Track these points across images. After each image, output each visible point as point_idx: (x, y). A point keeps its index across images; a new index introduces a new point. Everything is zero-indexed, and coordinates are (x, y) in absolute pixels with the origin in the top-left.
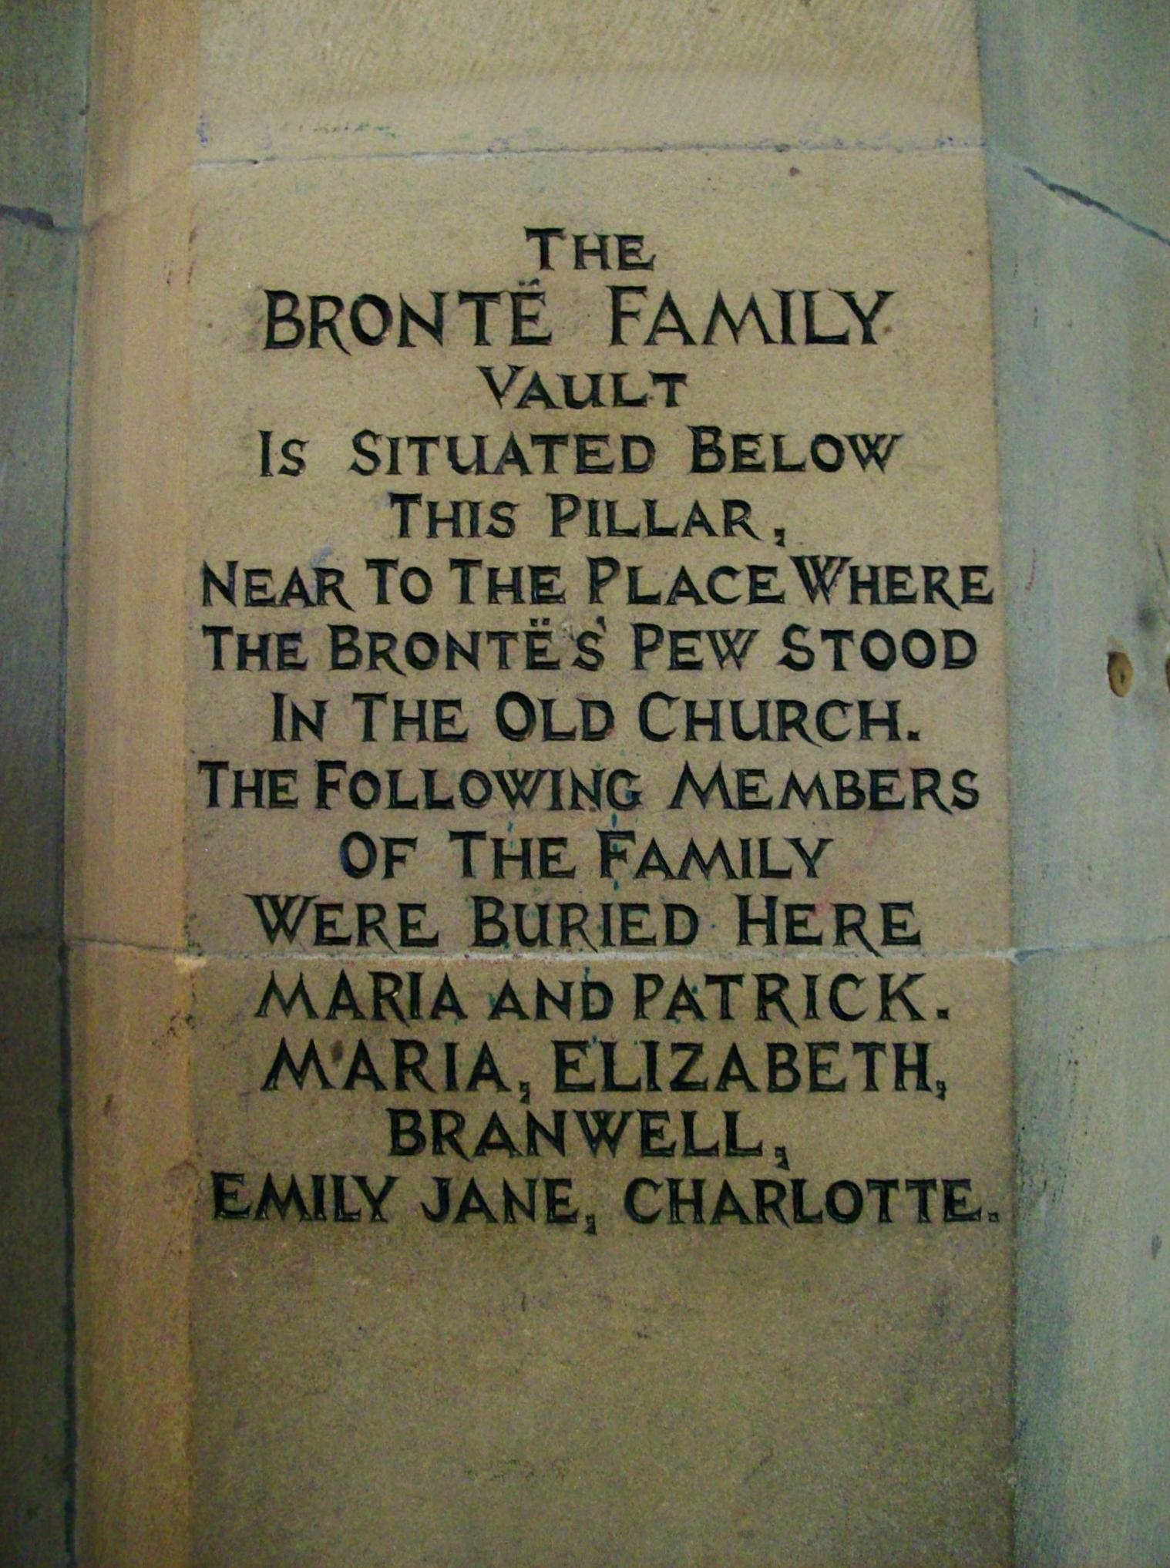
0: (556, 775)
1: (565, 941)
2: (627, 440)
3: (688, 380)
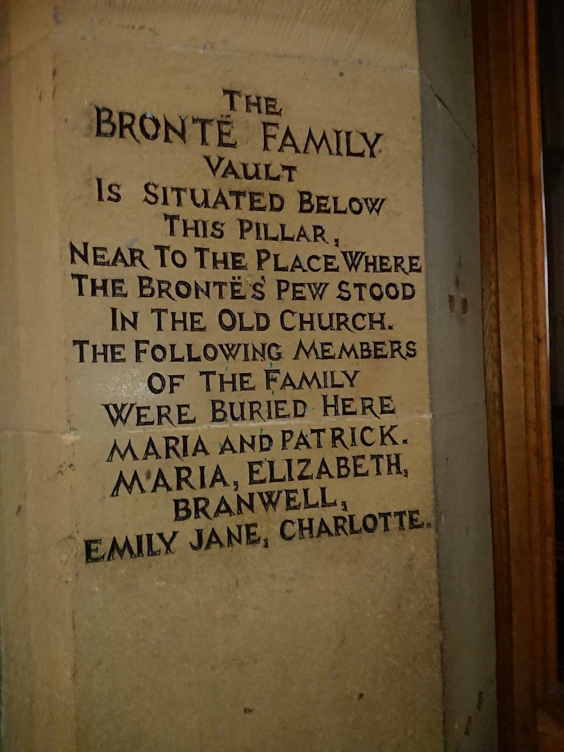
0: (246, 346)
1: (252, 418)
2: (272, 196)
3: (298, 169)
